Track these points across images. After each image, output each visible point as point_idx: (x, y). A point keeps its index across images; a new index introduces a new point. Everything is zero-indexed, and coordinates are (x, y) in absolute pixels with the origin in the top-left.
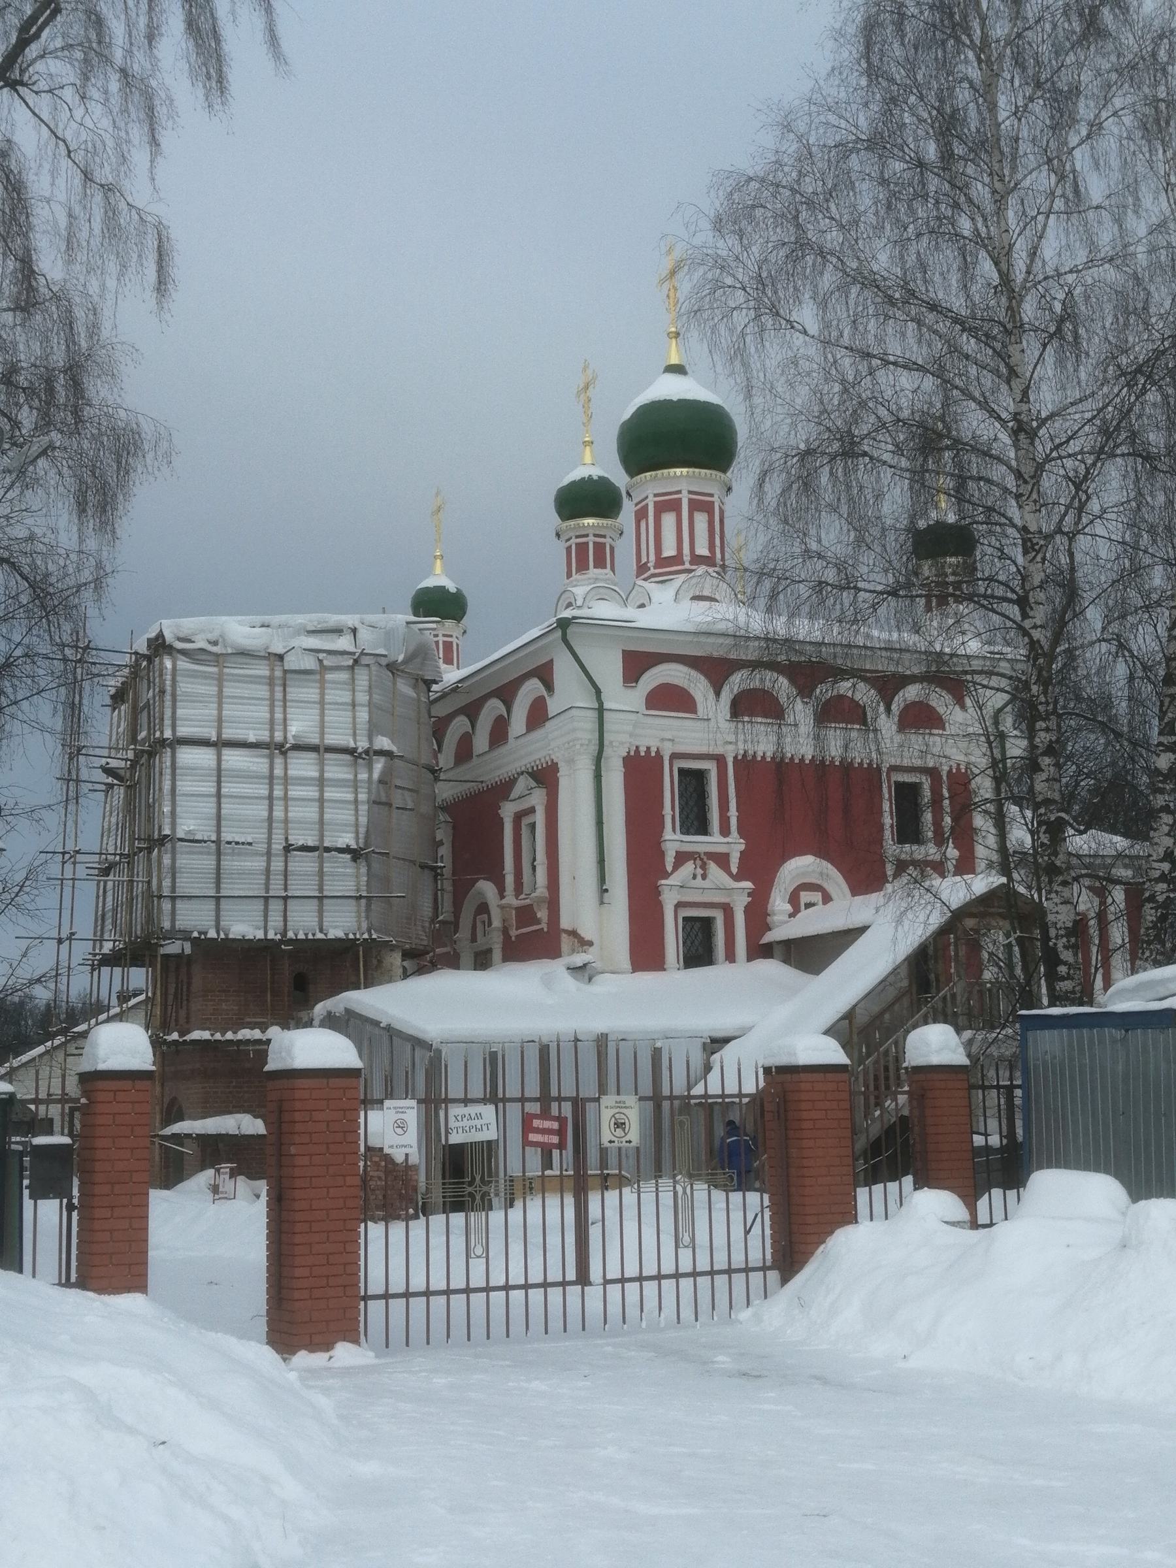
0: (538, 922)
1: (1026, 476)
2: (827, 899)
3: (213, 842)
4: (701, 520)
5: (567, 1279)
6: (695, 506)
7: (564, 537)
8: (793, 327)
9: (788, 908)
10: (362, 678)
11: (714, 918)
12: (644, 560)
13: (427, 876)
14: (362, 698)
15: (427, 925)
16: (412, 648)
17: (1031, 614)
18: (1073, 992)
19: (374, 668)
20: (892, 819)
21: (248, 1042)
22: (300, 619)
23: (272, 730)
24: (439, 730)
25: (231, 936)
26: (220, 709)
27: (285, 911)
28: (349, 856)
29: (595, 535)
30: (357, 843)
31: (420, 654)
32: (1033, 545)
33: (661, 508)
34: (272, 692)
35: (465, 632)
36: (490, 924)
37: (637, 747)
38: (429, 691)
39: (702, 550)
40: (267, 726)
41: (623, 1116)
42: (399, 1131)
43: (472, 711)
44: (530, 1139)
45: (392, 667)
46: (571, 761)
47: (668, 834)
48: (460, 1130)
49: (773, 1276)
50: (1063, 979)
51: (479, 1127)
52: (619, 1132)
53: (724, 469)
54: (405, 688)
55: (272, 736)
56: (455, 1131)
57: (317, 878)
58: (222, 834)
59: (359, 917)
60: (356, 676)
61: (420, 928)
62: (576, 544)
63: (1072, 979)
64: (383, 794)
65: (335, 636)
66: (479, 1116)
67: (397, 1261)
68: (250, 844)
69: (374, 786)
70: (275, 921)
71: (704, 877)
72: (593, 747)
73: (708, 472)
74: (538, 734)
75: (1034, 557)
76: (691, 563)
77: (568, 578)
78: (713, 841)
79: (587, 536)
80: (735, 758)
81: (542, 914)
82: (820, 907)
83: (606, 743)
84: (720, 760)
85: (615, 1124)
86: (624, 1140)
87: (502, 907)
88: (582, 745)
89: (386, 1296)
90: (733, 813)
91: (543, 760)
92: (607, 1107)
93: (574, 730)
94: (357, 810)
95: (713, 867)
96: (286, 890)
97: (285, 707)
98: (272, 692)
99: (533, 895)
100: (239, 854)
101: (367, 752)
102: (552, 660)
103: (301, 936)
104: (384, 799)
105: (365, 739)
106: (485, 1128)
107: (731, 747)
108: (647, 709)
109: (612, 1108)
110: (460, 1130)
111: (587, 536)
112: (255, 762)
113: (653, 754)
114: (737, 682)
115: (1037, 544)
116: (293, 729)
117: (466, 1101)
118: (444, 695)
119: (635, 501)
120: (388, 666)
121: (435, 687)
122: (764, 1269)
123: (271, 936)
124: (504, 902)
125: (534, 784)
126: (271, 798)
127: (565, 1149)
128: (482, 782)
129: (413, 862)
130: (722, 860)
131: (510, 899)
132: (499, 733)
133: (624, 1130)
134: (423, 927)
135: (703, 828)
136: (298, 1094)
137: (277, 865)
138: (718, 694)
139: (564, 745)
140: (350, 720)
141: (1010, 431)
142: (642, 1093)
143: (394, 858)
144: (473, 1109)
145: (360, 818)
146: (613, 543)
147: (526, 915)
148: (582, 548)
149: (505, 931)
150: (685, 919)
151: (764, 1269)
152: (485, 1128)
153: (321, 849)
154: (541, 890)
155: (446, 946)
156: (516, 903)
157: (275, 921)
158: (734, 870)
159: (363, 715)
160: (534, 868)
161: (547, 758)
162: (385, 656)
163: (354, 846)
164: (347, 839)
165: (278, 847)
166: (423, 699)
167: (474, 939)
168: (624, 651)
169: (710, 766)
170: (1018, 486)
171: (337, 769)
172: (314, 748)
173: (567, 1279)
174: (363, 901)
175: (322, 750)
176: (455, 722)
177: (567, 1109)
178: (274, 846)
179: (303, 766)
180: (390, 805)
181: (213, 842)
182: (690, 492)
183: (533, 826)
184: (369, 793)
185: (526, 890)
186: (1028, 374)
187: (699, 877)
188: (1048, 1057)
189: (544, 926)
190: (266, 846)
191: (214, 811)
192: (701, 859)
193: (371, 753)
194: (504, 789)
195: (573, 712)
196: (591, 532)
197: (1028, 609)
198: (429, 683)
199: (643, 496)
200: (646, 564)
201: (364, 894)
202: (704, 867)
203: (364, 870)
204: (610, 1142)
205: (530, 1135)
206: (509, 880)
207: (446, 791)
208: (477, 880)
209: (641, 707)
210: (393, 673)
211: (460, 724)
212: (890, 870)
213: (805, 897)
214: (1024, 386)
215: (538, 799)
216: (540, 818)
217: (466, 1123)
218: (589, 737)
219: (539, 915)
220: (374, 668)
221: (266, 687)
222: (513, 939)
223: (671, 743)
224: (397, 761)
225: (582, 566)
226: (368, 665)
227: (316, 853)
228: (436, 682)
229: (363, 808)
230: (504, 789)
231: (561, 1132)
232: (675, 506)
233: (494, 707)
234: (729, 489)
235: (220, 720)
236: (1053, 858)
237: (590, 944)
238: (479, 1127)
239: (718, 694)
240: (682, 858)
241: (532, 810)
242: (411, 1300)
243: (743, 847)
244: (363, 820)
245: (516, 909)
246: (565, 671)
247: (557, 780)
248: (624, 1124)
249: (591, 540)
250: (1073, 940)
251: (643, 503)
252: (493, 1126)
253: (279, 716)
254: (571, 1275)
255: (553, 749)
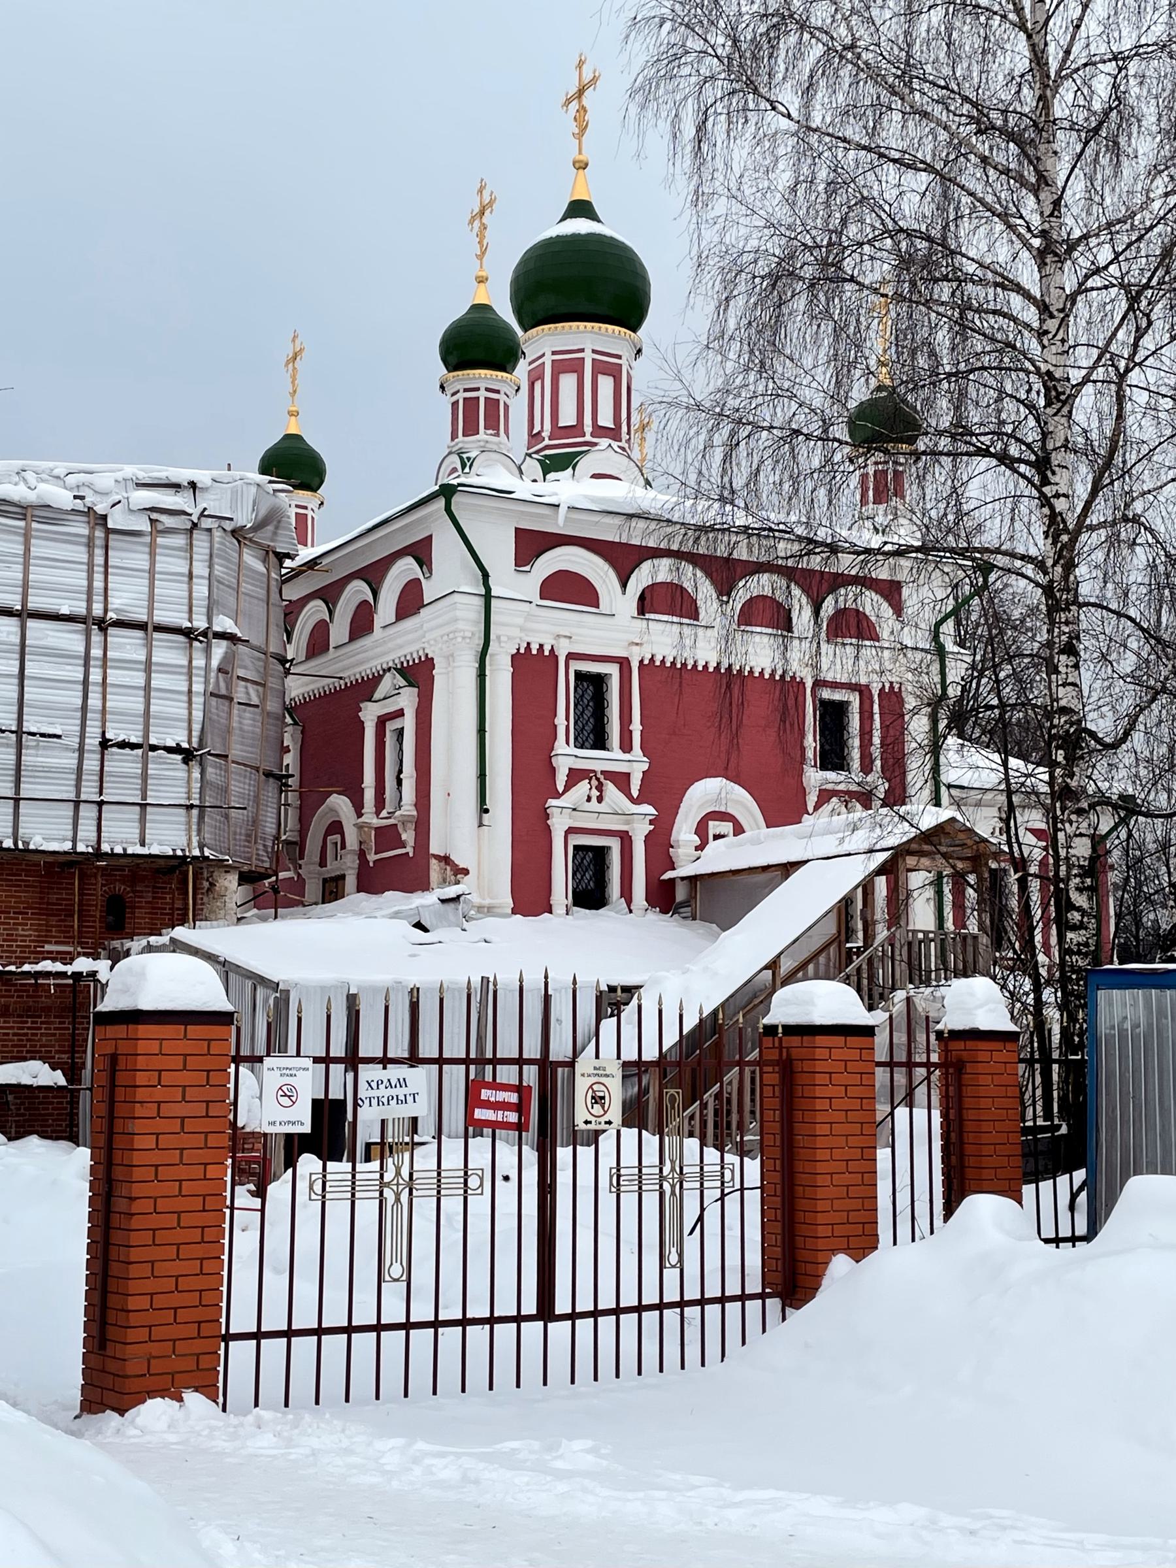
0: (403, 845)
1: (1053, 309)
2: (739, 830)
3: (12, 732)
4: (606, 384)
5: (523, 1313)
6: (600, 368)
7: (449, 391)
8: (774, 109)
9: (697, 840)
10: (201, 543)
11: (609, 848)
12: (536, 430)
13: (272, 785)
14: (200, 569)
15: (270, 844)
16: (263, 512)
17: (1053, 479)
18: (1086, 945)
19: (217, 534)
20: (815, 741)
21: (47, 974)
22: (131, 470)
23: (89, 601)
24: (291, 612)
25: (32, 847)
26: (26, 572)
27: (100, 819)
28: (180, 757)
29: (487, 390)
30: (190, 742)
31: (270, 519)
32: (1059, 394)
33: (560, 368)
34: (91, 555)
35: (322, 503)
36: (343, 847)
37: (528, 644)
38: (281, 567)
39: (606, 420)
40: (85, 597)
41: (603, 1088)
42: (285, 1101)
43: (329, 595)
44: (476, 1117)
45: (237, 534)
46: (450, 657)
47: (561, 746)
48: (374, 1102)
49: (773, 1304)
50: (1074, 928)
51: (402, 1097)
52: (597, 1109)
53: (634, 328)
54: (252, 560)
55: (89, 608)
56: (367, 1102)
57: (140, 781)
58: (25, 724)
59: (189, 830)
60: (194, 542)
61: (261, 847)
62: (465, 399)
63: (1086, 928)
64: (222, 685)
65: (172, 491)
66: (402, 1083)
67: (276, 1284)
68: (59, 737)
69: (213, 675)
70: (87, 832)
71: (600, 799)
72: (477, 642)
73: (617, 328)
74: (409, 623)
75: (1059, 410)
76: (592, 435)
77: (453, 439)
78: (611, 759)
79: (478, 389)
80: (641, 662)
81: (408, 836)
82: (731, 839)
83: (492, 637)
84: (624, 663)
85: (593, 1098)
86: (603, 1120)
87: (360, 827)
88: (464, 638)
89: (258, 1336)
90: (636, 727)
91: (415, 656)
92: (583, 1075)
93: (456, 620)
94: (190, 702)
95: (610, 788)
96: (101, 794)
97: (106, 574)
98: (91, 555)
99: (398, 813)
100: (44, 748)
101: (204, 634)
102: (431, 536)
103: (118, 850)
104: (223, 691)
105: (204, 618)
106: (410, 1099)
107: (635, 649)
108: (541, 598)
109: (589, 1076)
110: (374, 1102)
111: (478, 389)
112: (70, 639)
113: (547, 653)
114: (644, 576)
115: (1064, 393)
116: (115, 602)
117: (385, 1061)
118: (297, 573)
119: (529, 359)
120: (234, 532)
121: (288, 563)
122: (762, 1296)
123: (81, 848)
124: (360, 820)
125: (402, 682)
126: (86, 682)
127: (527, 1131)
128: (341, 678)
129: (257, 769)
130: (622, 780)
131: (369, 817)
132: (362, 623)
133: (603, 1106)
134: (265, 846)
135: (600, 742)
136: (142, 1047)
137: (91, 763)
138: (624, 585)
139: (442, 637)
140: (186, 594)
141: (1035, 253)
142: (624, 1057)
143: (233, 762)
144: (395, 1072)
145: (194, 712)
146: (508, 401)
147: (387, 836)
148: (470, 404)
149: (362, 854)
150: (576, 848)
151: (762, 1296)
152: (410, 1099)
153: (146, 747)
154: (408, 807)
155: (289, 870)
156: (376, 822)
157: (87, 832)
158: (635, 793)
159: (201, 590)
160: (399, 782)
161: (421, 653)
162: (231, 519)
163: (185, 745)
164: (177, 737)
165: (93, 741)
166: (273, 575)
167: (323, 863)
168: (518, 531)
169: (613, 670)
170: (1042, 321)
171: (168, 652)
172: (141, 626)
173: (523, 1313)
174: (195, 812)
175: (150, 628)
176: (306, 609)
177: (531, 1075)
178: (87, 741)
179: (126, 645)
180: (231, 699)
181: (12, 732)
182: (594, 351)
183: (400, 733)
184: (206, 682)
185: (389, 807)
186: (1060, 184)
187: (594, 799)
188: (1128, 1025)
189: (409, 850)
190: (77, 740)
191: (15, 695)
192: (598, 779)
193: (210, 635)
194: (366, 688)
195: (456, 597)
196: (483, 386)
197: (1049, 473)
198: (281, 557)
199: (540, 354)
200: (539, 433)
201: (197, 802)
202: (600, 787)
203: (196, 774)
204: (587, 1122)
205: (477, 1111)
206: (369, 795)
207: (297, 688)
208: (329, 794)
209: (535, 595)
210: (239, 542)
211: (316, 610)
212: (812, 799)
213: (714, 827)
214: (1056, 197)
215: (407, 700)
216: (409, 723)
217: (383, 1092)
218: (474, 629)
219: (404, 837)
220: (217, 534)
221: (84, 549)
222: (371, 864)
223: (567, 640)
224: (241, 648)
225: (471, 429)
226: (209, 530)
227: (139, 752)
228: (288, 556)
229: (198, 701)
230: (366, 688)
231: (520, 1108)
232: (576, 367)
233: (358, 590)
234: (639, 351)
235: (25, 585)
236: (1069, 780)
237: (466, 872)
238: (402, 1097)
239: (624, 585)
240: (575, 776)
241: (400, 713)
242: (284, 1327)
243: (646, 767)
244: (198, 715)
245: (377, 829)
246: (446, 548)
247: (432, 679)
248: (603, 1098)
249: (482, 395)
250: (1088, 881)
251: (540, 361)
252: (422, 1099)
253: (98, 584)
254: (530, 1306)
255: (428, 642)
